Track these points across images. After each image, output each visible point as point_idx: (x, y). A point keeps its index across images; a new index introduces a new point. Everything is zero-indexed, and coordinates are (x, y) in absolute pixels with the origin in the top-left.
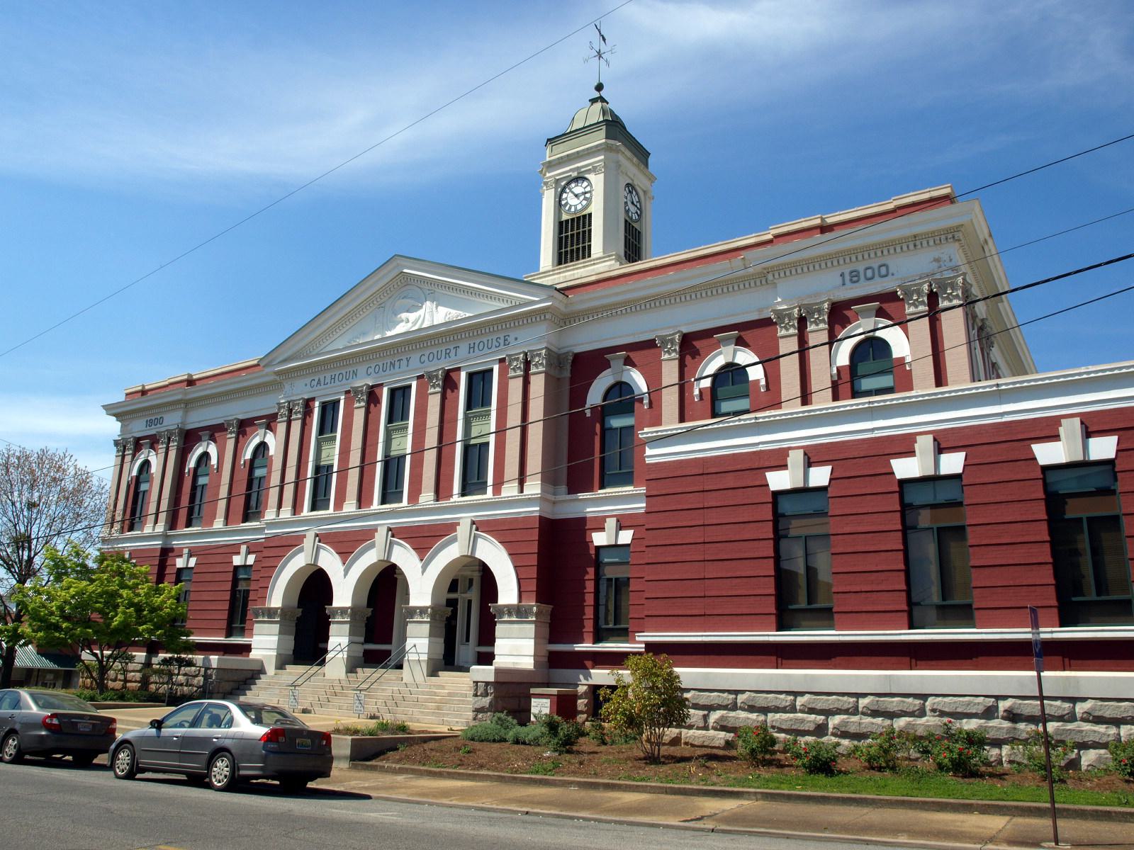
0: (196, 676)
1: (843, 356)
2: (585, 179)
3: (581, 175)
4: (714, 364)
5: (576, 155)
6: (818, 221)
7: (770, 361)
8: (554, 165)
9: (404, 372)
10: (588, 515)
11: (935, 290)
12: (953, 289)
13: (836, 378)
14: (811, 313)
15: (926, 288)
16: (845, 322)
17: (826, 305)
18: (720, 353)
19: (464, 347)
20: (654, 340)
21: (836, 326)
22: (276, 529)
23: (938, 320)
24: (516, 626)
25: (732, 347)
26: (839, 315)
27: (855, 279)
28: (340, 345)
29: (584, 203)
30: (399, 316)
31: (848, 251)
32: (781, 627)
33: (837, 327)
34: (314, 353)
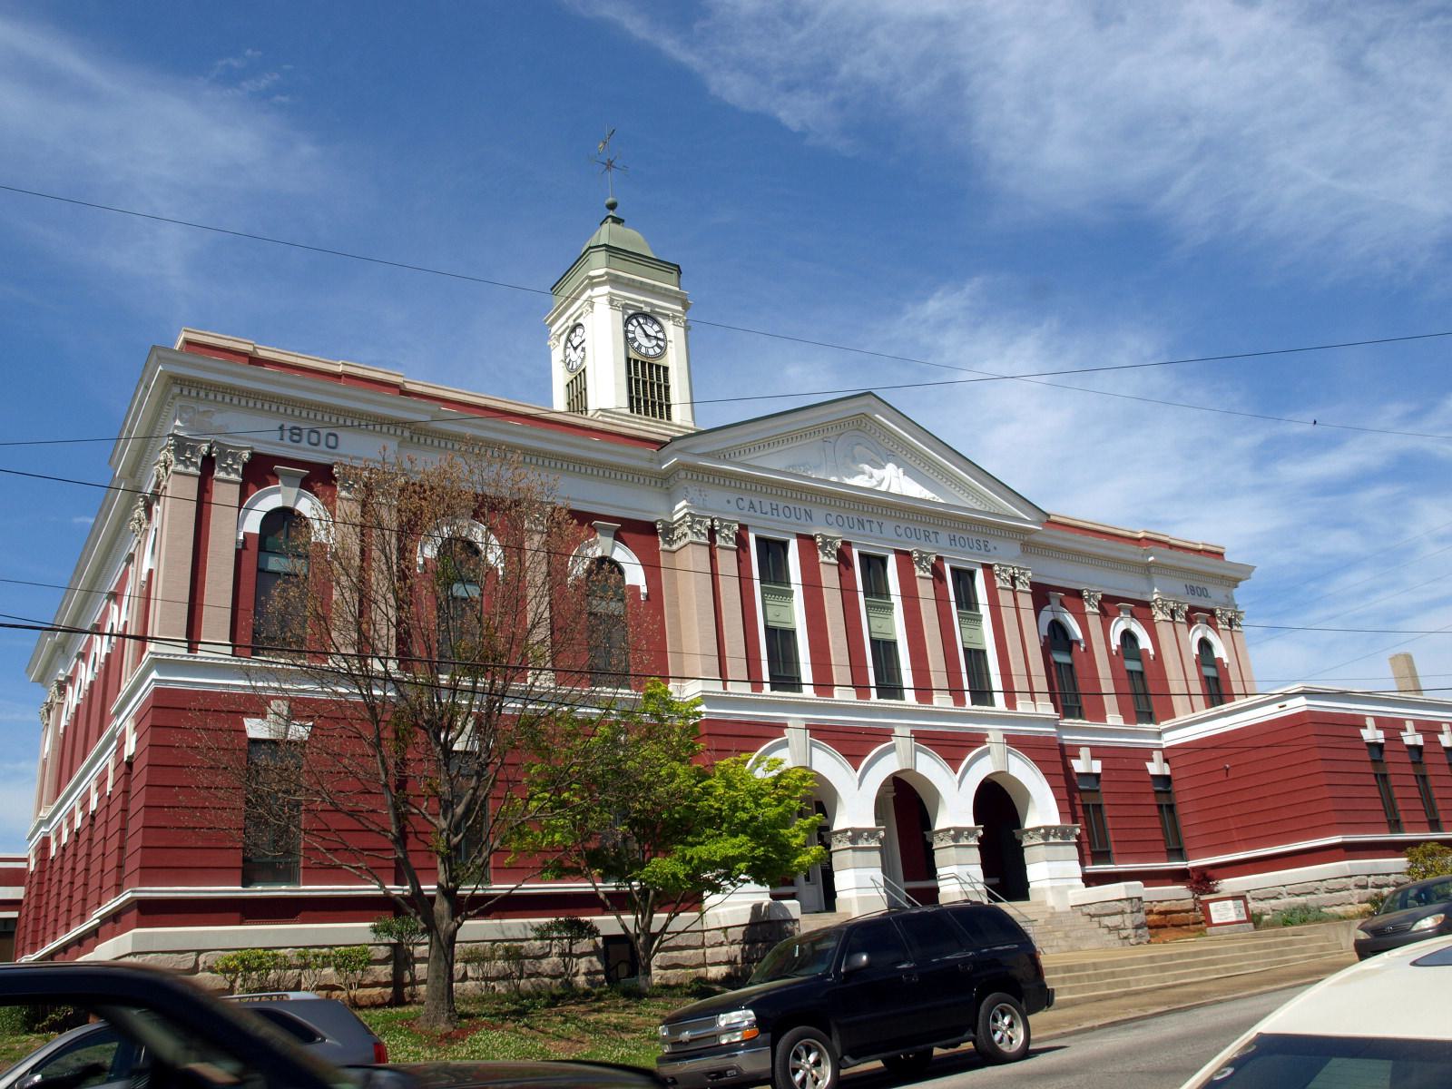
0: (546, 955)
1: (253, 524)
2: (656, 322)
3: (654, 315)
4: (272, 501)
5: (638, 285)
6: (250, 348)
7: (514, 550)
8: (622, 283)
9: (901, 542)
10: (1065, 743)
11: (214, 455)
12: (192, 453)
13: (240, 547)
14: (224, 454)
15: (205, 448)
16: (262, 483)
17: (246, 455)
18: (278, 491)
19: (944, 537)
20: (331, 467)
21: (251, 484)
22: (821, 714)
23: (208, 492)
24: (1061, 848)
25: (295, 490)
26: (259, 472)
27: (296, 438)
28: (773, 464)
29: (658, 350)
30: (861, 466)
31: (562, 456)
32: (246, 882)
33: (251, 486)
34: (738, 460)
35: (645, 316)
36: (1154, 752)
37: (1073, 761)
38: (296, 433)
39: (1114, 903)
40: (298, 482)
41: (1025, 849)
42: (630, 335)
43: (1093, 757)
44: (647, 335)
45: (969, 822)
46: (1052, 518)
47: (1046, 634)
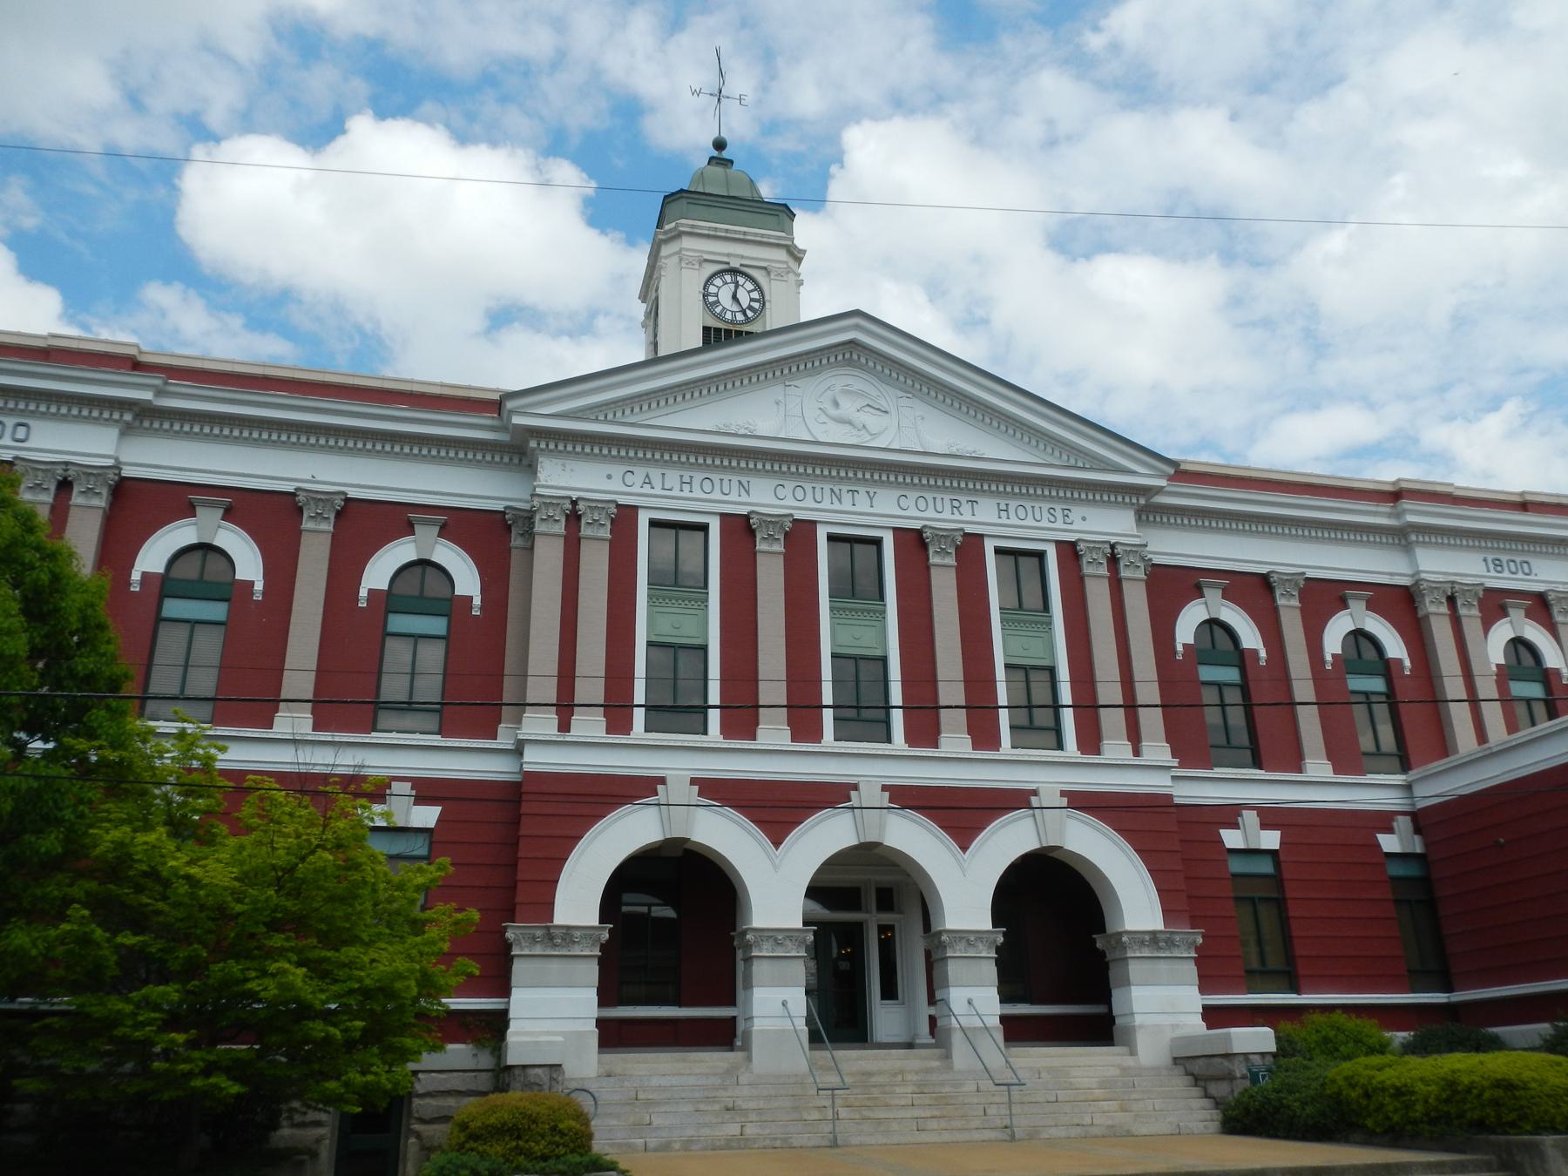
35: (734, 272)
36: (1245, 812)
37: (1222, 832)
38: (1498, 564)
39: (1218, 1060)
40: (220, 512)
41: (950, 962)
42: (711, 299)
43: (1264, 826)
44: (734, 297)
45: (986, 923)
46: (1183, 467)
47: (1502, 662)
